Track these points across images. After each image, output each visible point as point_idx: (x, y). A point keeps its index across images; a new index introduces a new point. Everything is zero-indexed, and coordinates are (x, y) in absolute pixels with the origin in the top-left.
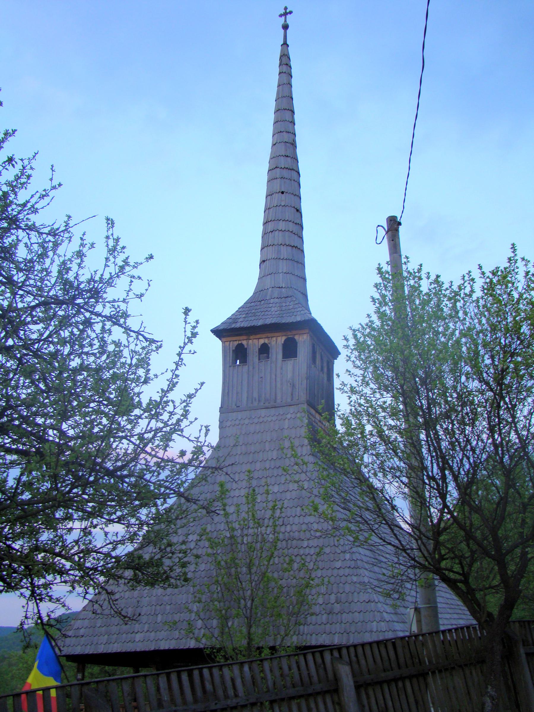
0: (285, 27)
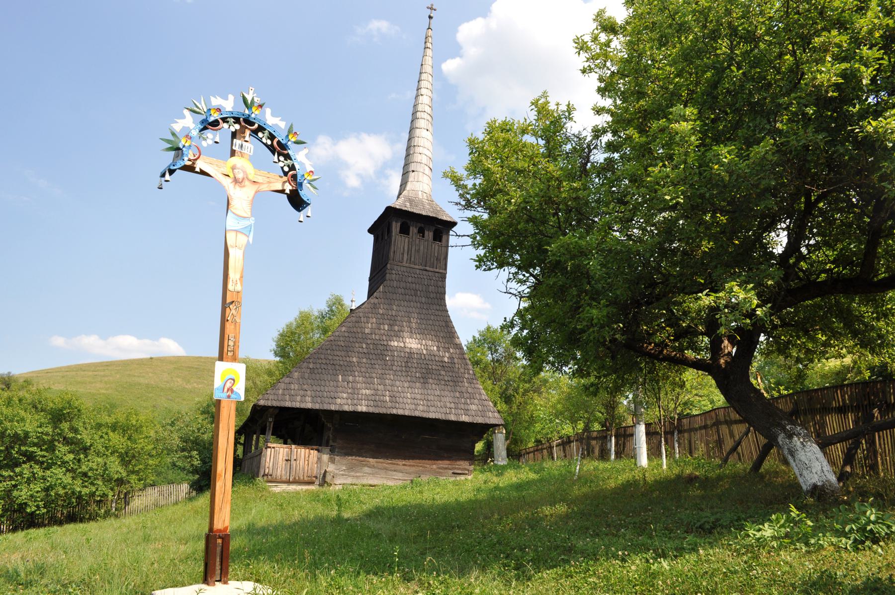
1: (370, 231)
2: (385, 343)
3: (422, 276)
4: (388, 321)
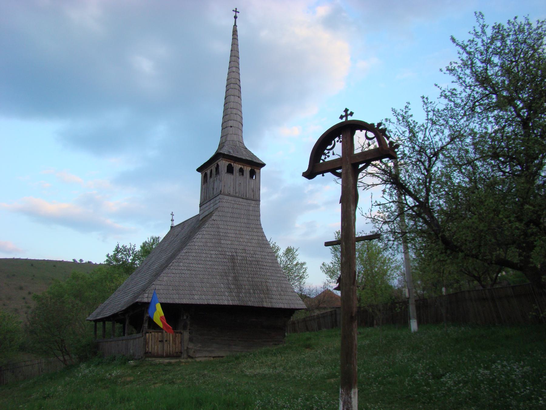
0: (236, 17)
1: (199, 170)
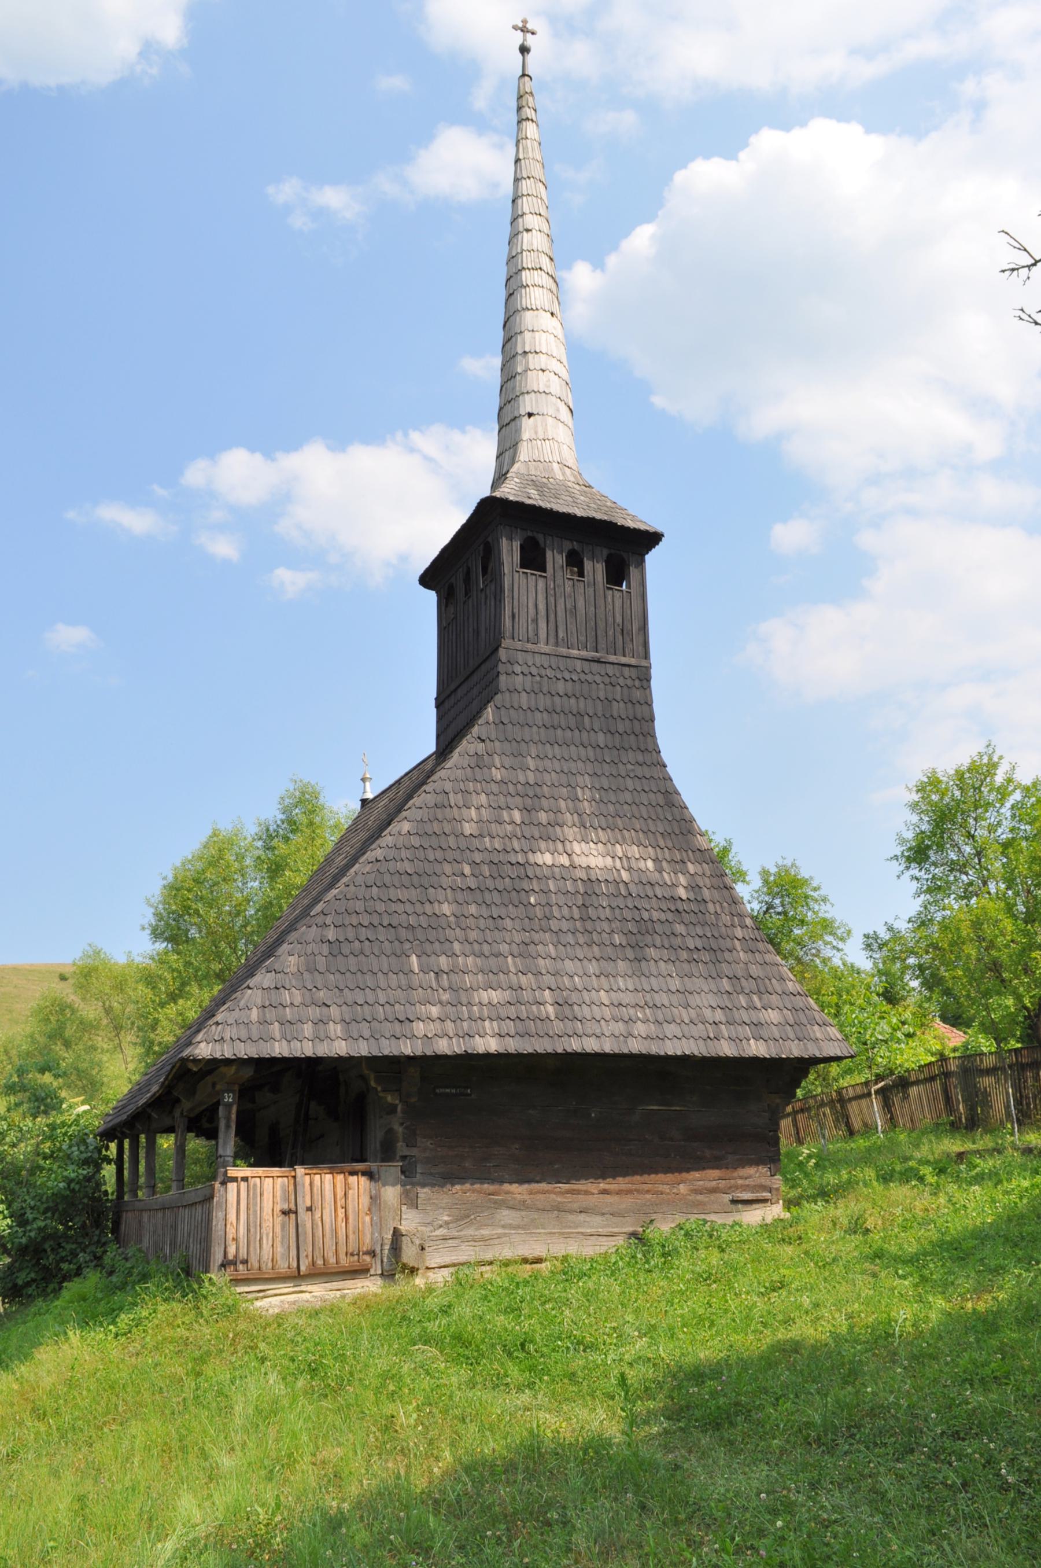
1: (427, 579)
2: (520, 858)
3: (590, 678)
4: (518, 799)
